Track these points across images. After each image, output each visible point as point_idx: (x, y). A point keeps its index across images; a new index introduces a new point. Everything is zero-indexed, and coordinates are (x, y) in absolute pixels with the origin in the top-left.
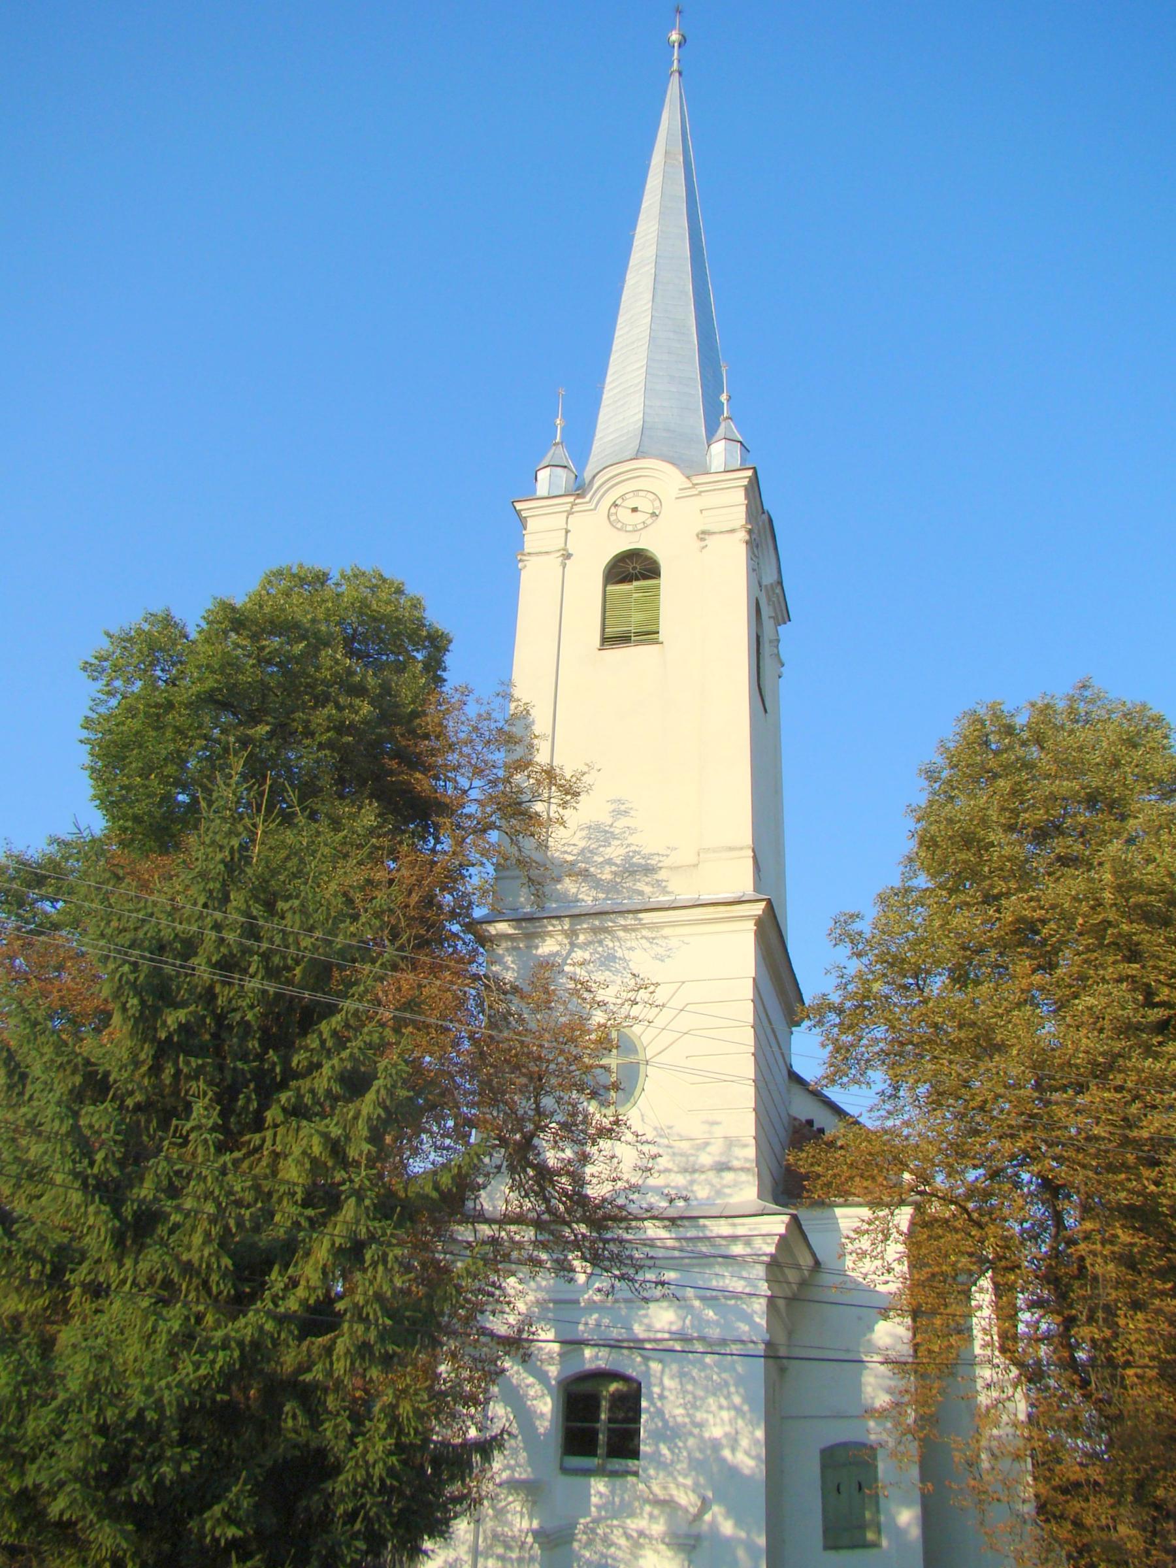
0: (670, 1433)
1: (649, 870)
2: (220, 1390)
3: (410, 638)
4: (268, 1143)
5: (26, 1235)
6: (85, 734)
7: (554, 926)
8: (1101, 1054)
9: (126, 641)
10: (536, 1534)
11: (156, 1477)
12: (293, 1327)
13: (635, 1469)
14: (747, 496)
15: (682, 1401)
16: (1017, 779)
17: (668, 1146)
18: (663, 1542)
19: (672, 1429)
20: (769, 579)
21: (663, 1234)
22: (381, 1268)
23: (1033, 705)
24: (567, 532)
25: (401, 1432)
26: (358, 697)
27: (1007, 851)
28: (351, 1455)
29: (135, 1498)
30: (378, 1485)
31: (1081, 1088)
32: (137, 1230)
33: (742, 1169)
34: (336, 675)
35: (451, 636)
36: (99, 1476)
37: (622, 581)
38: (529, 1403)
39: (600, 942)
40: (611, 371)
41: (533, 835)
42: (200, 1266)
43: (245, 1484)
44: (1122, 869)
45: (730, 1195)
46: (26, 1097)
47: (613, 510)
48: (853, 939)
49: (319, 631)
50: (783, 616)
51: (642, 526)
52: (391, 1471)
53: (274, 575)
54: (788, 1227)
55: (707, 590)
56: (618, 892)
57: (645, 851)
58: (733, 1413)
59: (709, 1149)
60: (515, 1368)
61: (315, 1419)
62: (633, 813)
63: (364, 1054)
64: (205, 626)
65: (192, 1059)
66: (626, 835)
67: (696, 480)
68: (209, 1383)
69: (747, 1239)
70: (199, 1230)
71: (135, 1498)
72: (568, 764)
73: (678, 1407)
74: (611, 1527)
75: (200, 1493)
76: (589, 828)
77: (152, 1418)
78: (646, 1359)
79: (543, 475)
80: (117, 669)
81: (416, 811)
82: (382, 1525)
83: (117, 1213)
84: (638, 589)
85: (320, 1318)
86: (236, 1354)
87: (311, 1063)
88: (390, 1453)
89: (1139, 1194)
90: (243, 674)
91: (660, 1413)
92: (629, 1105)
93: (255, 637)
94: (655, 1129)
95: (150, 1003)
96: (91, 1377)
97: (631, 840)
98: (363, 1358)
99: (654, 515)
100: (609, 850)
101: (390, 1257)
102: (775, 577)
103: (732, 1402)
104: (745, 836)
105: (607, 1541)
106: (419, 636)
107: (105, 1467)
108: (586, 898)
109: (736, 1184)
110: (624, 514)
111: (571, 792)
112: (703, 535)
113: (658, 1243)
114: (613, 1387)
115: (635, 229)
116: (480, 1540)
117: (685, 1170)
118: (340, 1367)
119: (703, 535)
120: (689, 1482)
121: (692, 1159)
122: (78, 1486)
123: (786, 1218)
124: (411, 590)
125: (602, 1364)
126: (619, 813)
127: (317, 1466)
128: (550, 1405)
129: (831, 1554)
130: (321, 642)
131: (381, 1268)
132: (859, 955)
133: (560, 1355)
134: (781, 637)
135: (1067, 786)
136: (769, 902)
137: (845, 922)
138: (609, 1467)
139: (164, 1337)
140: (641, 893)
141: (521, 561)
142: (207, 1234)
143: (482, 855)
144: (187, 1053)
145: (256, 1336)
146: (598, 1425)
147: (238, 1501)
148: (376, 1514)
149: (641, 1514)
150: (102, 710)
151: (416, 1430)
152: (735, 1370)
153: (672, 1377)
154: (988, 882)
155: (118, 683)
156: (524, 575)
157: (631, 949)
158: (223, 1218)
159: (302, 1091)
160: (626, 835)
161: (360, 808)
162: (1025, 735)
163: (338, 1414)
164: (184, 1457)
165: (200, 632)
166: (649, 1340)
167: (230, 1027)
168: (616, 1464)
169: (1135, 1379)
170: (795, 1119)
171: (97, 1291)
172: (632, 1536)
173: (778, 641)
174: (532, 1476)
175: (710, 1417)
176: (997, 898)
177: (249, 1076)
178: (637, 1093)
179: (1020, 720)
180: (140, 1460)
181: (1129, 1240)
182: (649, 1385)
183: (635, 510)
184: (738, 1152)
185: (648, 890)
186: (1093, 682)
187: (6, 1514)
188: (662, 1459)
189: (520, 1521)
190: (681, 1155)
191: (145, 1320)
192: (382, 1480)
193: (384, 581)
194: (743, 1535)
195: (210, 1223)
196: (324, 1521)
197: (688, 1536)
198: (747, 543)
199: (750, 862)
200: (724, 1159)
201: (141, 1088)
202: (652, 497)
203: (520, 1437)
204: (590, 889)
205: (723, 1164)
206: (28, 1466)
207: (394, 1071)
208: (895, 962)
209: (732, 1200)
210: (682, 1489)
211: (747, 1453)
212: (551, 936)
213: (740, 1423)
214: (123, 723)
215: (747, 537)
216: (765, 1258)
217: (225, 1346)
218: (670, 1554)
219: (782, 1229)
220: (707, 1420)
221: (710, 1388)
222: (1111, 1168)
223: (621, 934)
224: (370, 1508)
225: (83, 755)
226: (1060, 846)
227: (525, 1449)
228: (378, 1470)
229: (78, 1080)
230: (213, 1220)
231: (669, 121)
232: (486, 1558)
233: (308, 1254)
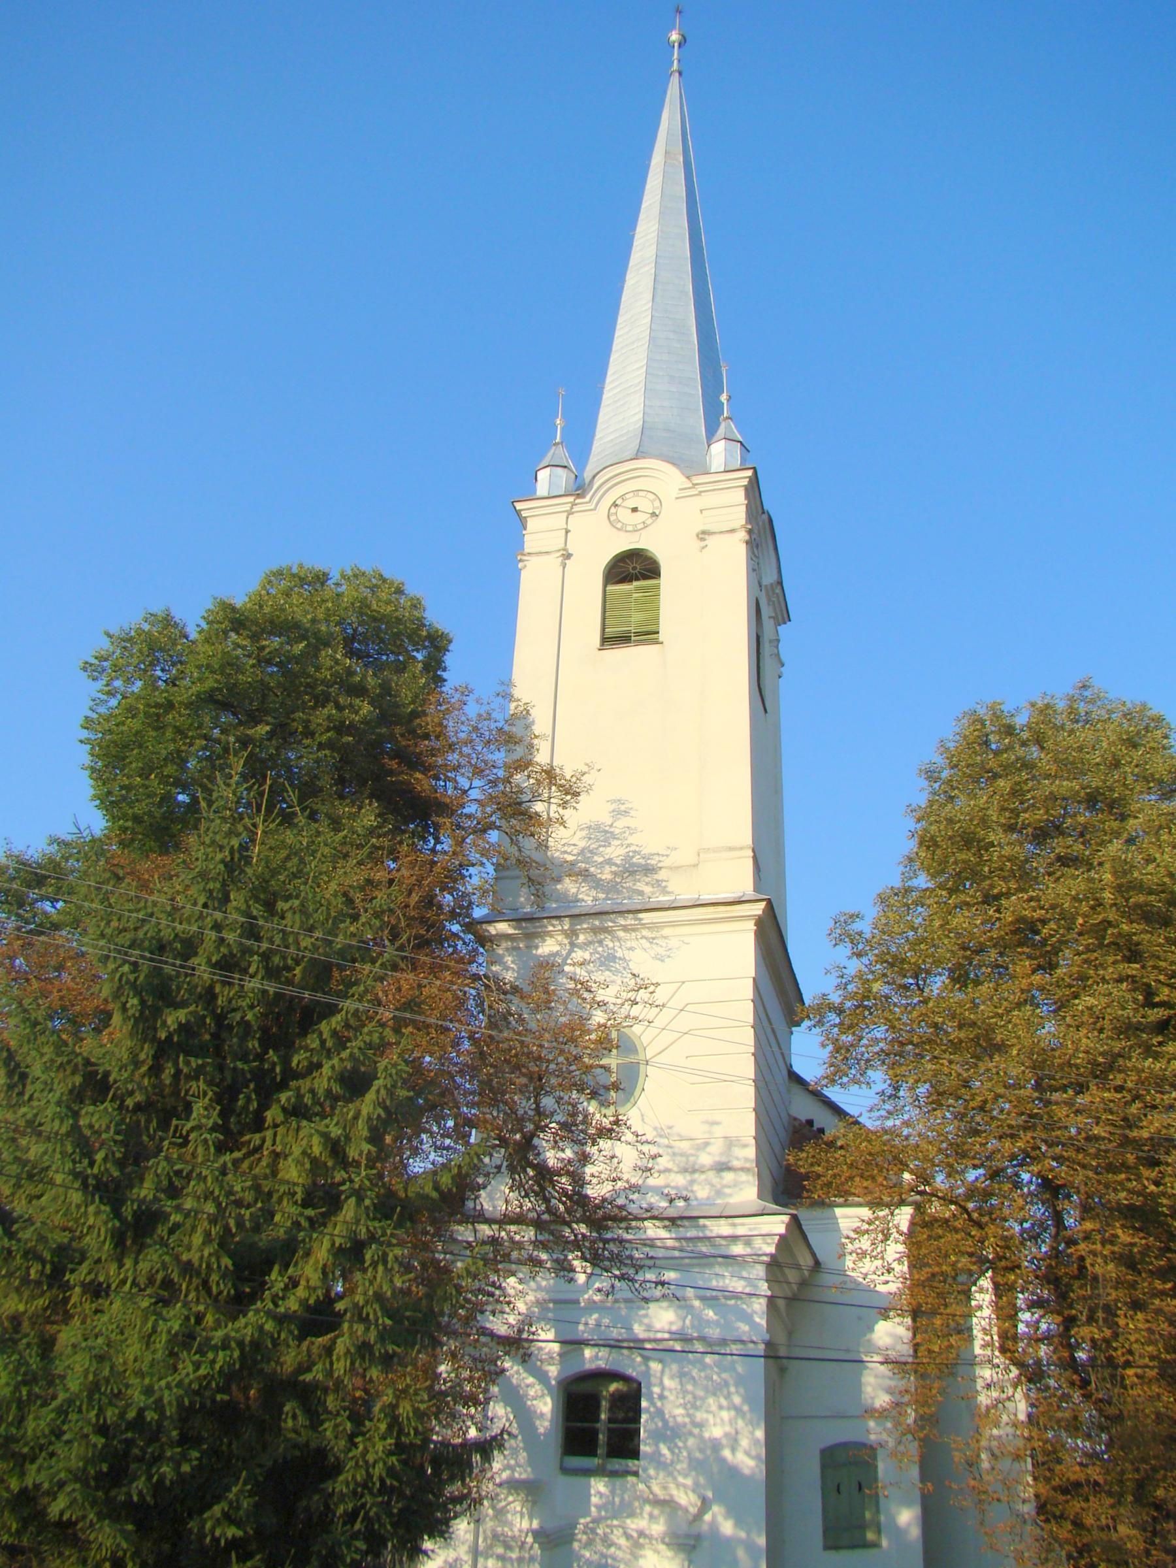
0: (670, 1433)
1: (649, 870)
4: (268, 1143)
5: (26, 1235)
6: (85, 734)
7: (554, 926)
8: (1101, 1054)
9: (126, 641)
10: (536, 1534)
11: (156, 1477)
12: (293, 1327)
13: (635, 1469)
14: (747, 496)
15: (682, 1401)
16: (1017, 779)
17: (668, 1146)
18: (663, 1542)
19: (672, 1429)
20: (769, 578)
21: (663, 1233)
22: (381, 1268)
23: (1033, 705)
24: (567, 532)
25: (401, 1431)
26: (358, 697)
27: (1007, 851)
28: (350, 1455)
29: (135, 1498)
30: (378, 1485)
31: (1081, 1088)
32: (137, 1230)
33: (742, 1169)
34: (336, 675)
35: (451, 636)
36: (99, 1476)
38: (529, 1403)
39: (600, 942)
40: (610, 372)
41: (533, 835)
42: (200, 1266)
43: (245, 1484)
44: (1122, 869)
45: (730, 1195)
46: (26, 1097)
47: (613, 510)
48: (853, 939)
49: (319, 631)
50: (783, 616)
51: (642, 526)
52: (391, 1471)
53: (274, 574)
54: (788, 1226)
55: (707, 591)
56: (619, 892)
58: (733, 1413)
59: (709, 1149)
60: (515, 1368)
61: (315, 1419)
62: (632, 813)
63: (364, 1054)
64: (205, 626)
65: (192, 1059)
67: (696, 480)
68: (209, 1383)
69: (747, 1240)
70: (199, 1230)
71: (135, 1498)
72: (568, 764)
73: (678, 1407)
74: (611, 1527)
75: (201, 1492)
76: (589, 828)
78: (646, 1359)
79: (543, 475)
80: (116, 668)
81: (416, 811)
82: (382, 1525)
83: (117, 1213)
84: (638, 589)
85: (320, 1318)
86: (236, 1354)
87: (311, 1063)
88: (390, 1453)
90: (243, 673)
91: (660, 1413)
92: (629, 1105)
93: (255, 637)
94: (655, 1129)
95: (150, 1003)
96: (91, 1377)
97: (630, 840)
98: (363, 1358)
99: (654, 515)
100: (609, 850)
101: (390, 1257)
104: (745, 836)
105: (607, 1541)
106: (419, 636)
108: (586, 898)
110: (624, 514)
111: (571, 792)
112: (703, 535)
113: (658, 1243)
114: (613, 1387)
116: (480, 1540)
117: (685, 1170)
118: (340, 1367)
119: (703, 535)
120: (689, 1482)
122: (78, 1486)
123: (786, 1218)
124: (411, 590)
125: (602, 1364)
126: (619, 813)
127: (318, 1466)
128: (550, 1405)
129: (832, 1554)
131: (381, 1268)
132: (859, 955)
133: (560, 1355)
134: (781, 637)
135: (1066, 786)
136: (769, 903)
138: (609, 1467)
139: (164, 1337)
140: (641, 893)
141: (521, 561)
142: (207, 1234)
143: (482, 855)
144: (187, 1053)
146: (598, 1425)
147: (238, 1501)
148: (376, 1514)
149: (641, 1514)
150: (102, 710)
151: (416, 1429)
152: (735, 1369)
153: (672, 1377)
154: (988, 882)
155: (118, 683)
157: (631, 949)
159: (302, 1091)
161: (360, 808)
162: (1025, 735)
163: (338, 1414)
164: (185, 1457)
165: (200, 632)
166: (649, 1340)
167: (230, 1028)
168: (616, 1464)
169: (1135, 1379)
170: (795, 1119)
171: (97, 1291)
172: (632, 1536)
173: (778, 641)
174: (532, 1476)
175: (710, 1417)
176: (997, 898)
177: (249, 1076)
178: (637, 1093)
179: (1021, 720)
181: (1129, 1240)
182: (649, 1385)
183: (635, 510)
184: (738, 1152)
185: (648, 890)
186: (1094, 682)
188: (662, 1459)
189: (520, 1521)
190: (681, 1155)
191: (145, 1320)
192: (382, 1480)
193: (384, 581)
194: (743, 1535)
195: (210, 1222)
196: (324, 1521)
197: (688, 1536)
198: (747, 543)
199: (750, 862)
200: (724, 1159)
201: (141, 1088)
202: (652, 497)
203: (520, 1437)
205: (723, 1164)
206: (28, 1466)
207: (394, 1071)
208: (895, 962)
209: (732, 1200)
211: (747, 1453)
212: (552, 936)
213: (740, 1423)
214: (123, 723)
215: (747, 537)
216: (765, 1258)
217: (225, 1346)
218: (670, 1554)
219: (782, 1229)
220: (707, 1420)
221: (710, 1388)
222: (1111, 1168)
223: (621, 934)
224: (370, 1508)
225: (83, 755)
226: (1060, 846)
227: (525, 1449)
228: (378, 1470)
229: (78, 1080)
230: (213, 1220)
231: (669, 121)
232: (486, 1558)
233: (308, 1254)
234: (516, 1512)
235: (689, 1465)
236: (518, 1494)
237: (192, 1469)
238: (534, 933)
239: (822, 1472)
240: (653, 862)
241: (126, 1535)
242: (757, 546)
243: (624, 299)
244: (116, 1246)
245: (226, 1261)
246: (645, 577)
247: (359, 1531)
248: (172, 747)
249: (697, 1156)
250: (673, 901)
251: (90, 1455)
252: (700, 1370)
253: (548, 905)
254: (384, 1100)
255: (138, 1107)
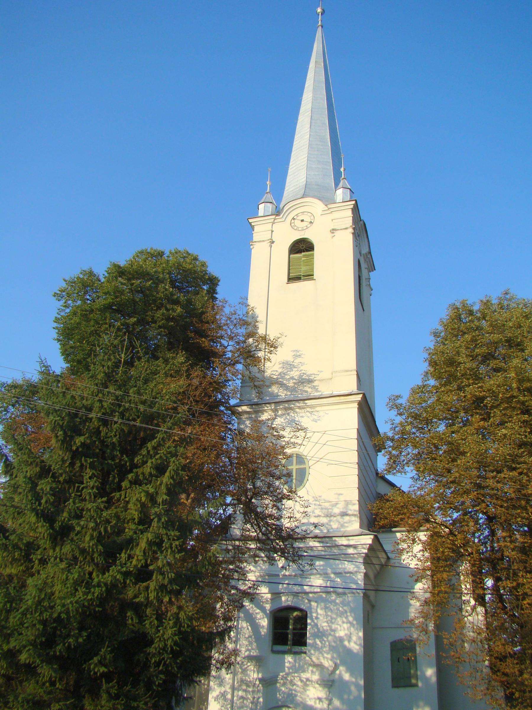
0: (320, 634)
1: (310, 381)
2: (98, 606)
3: (201, 279)
4: (123, 497)
5: (12, 537)
6: (55, 325)
7: (267, 407)
8: (508, 454)
9: (72, 283)
10: (260, 680)
11: (67, 644)
12: (132, 578)
13: (305, 651)
14: (353, 213)
15: (326, 620)
16: (474, 334)
17: (319, 505)
18: (318, 683)
19: (321, 632)
20: (365, 251)
21: (317, 544)
22: (169, 551)
23: (481, 301)
24: (272, 231)
25: (181, 626)
26: (175, 305)
27: (468, 365)
28: (157, 635)
29: (58, 654)
30: (170, 649)
31: (499, 472)
32: (60, 535)
33: (353, 515)
34: (166, 295)
35: (219, 278)
36: (41, 643)
37: (297, 253)
38: (257, 621)
39: (288, 414)
40: (292, 160)
41: (256, 366)
42: (89, 550)
43: (108, 647)
44: (519, 372)
45: (347, 527)
46: (14, 476)
47: (293, 221)
48: (397, 407)
49: (159, 277)
50: (372, 268)
52: (176, 643)
53: (140, 253)
54: (373, 540)
55: (336, 257)
56: (296, 392)
57: (308, 373)
58: (349, 625)
59: (338, 506)
60: (251, 605)
61: (141, 618)
62: (302, 356)
63: (166, 457)
64: (107, 275)
65: (88, 459)
67: (330, 206)
68: (93, 603)
69: (355, 547)
70: (88, 534)
71: (58, 654)
72: (272, 336)
73: (324, 622)
74: (294, 677)
75: (88, 651)
76: (283, 363)
77: (64, 617)
78: (310, 601)
79: (261, 207)
80: (69, 295)
81: (203, 356)
82: (173, 668)
83: (52, 527)
84: (304, 256)
85: (143, 574)
86: (104, 589)
87: (143, 461)
88: (175, 634)
89: (527, 519)
90: (124, 295)
91: (316, 625)
92: (301, 487)
93: (129, 279)
94: (313, 497)
95: (69, 434)
96: (37, 598)
97: (302, 368)
98: (162, 592)
99: (311, 222)
100: (292, 373)
101: (174, 545)
102: (368, 250)
103: (348, 620)
104: (352, 364)
105: (292, 683)
106: (205, 278)
107: (44, 639)
108: (282, 394)
109: (350, 522)
110: (297, 223)
111: (273, 346)
112: (333, 231)
113: (315, 549)
114: (295, 614)
116: (236, 683)
117: (327, 516)
118: (152, 596)
119: (333, 231)
120: (329, 656)
121: (330, 510)
122: (31, 647)
123: (372, 537)
124: (201, 258)
125: (290, 603)
126: (297, 356)
127: (143, 640)
128: (266, 622)
129: (396, 690)
130: (158, 281)
131: (169, 551)
132: (401, 414)
133: (271, 599)
134: (371, 277)
135: (496, 337)
136: (364, 397)
137: (394, 399)
138: (293, 650)
139: (71, 581)
140: (307, 392)
141: (251, 245)
142: (92, 536)
143: (233, 375)
144: (86, 457)
145: (113, 581)
146: (289, 631)
147: (105, 655)
148: (170, 662)
149: (308, 671)
150: (63, 314)
151: (188, 625)
152: (350, 606)
153: (321, 609)
154: (460, 380)
155: (70, 302)
156: (253, 251)
157: (302, 417)
158: (98, 528)
159: (139, 474)
161: (177, 354)
162: (479, 315)
163: (151, 617)
164: (80, 635)
165: (105, 278)
166: (311, 593)
167: (107, 446)
168: (297, 649)
169: (527, 606)
170: (379, 494)
171: (43, 562)
172: (303, 681)
173: (370, 279)
174: (258, 654)
175: (339, 627)
176: (463, 387)
177: (114, 467)
178: (305, 482)
179: (476, 308)
180: (60, 636)
181: (522, 540)
182: (311, 612)
183: (302, 221)
184: (350, 507)
185: (309, 390)
186: (510, 291)
187: (2, 661)
188: (317, 646)
189: (254, 674)
190: (325, 509)
191: (63, 573)
192: (172, 648)
193: (189, 254)
194: (354, 680)
195: (93, 530)
196: (146, 665)
197: (328, 681)
198: (353, 234)
199: (355, 376)
200: (344, 510)
201: (65, 472)
203: (253, 637)
205: (344, 512)
206: (11, 639)
207: (177, 463)
208: (416, 417)
209: (348, 529)
210: (326, 659)
211: (355, 643)
212: (266, 412)
213: (352, 629)
214: (72, 319)
215: (353, 231)
216: (363, 555)
217: (99, 585)
218: (320, 689)
219: (370, 542)
220: (337, 628)
221: (339, 613)
222: (514, 507)
223: (298, 410)
224: (167, 661)
225: (54, 334)
226: (493, 363)
227: (255, 642)
228: (169, 642)
229: (38, 469)
230: (94, 529)
231: (317, 47)
232: (238, 691)
233: (137, 545)
234: (251, 670)
235: (329, 648)
236: (252, 662)
237: (83, 640)
239: (391, 653)
241: (55, 671)
242: (359, 236)
244: (52, 543)
245: (100, 547)
246: (308, 251)
247: (162, 670)
248: (93, 328)
249: (332, 509)
250: (321, 395)
251: (37, 633)
252: (334, 606)
253: (265, 398)
254: (173, 476)
255: (65, 481)
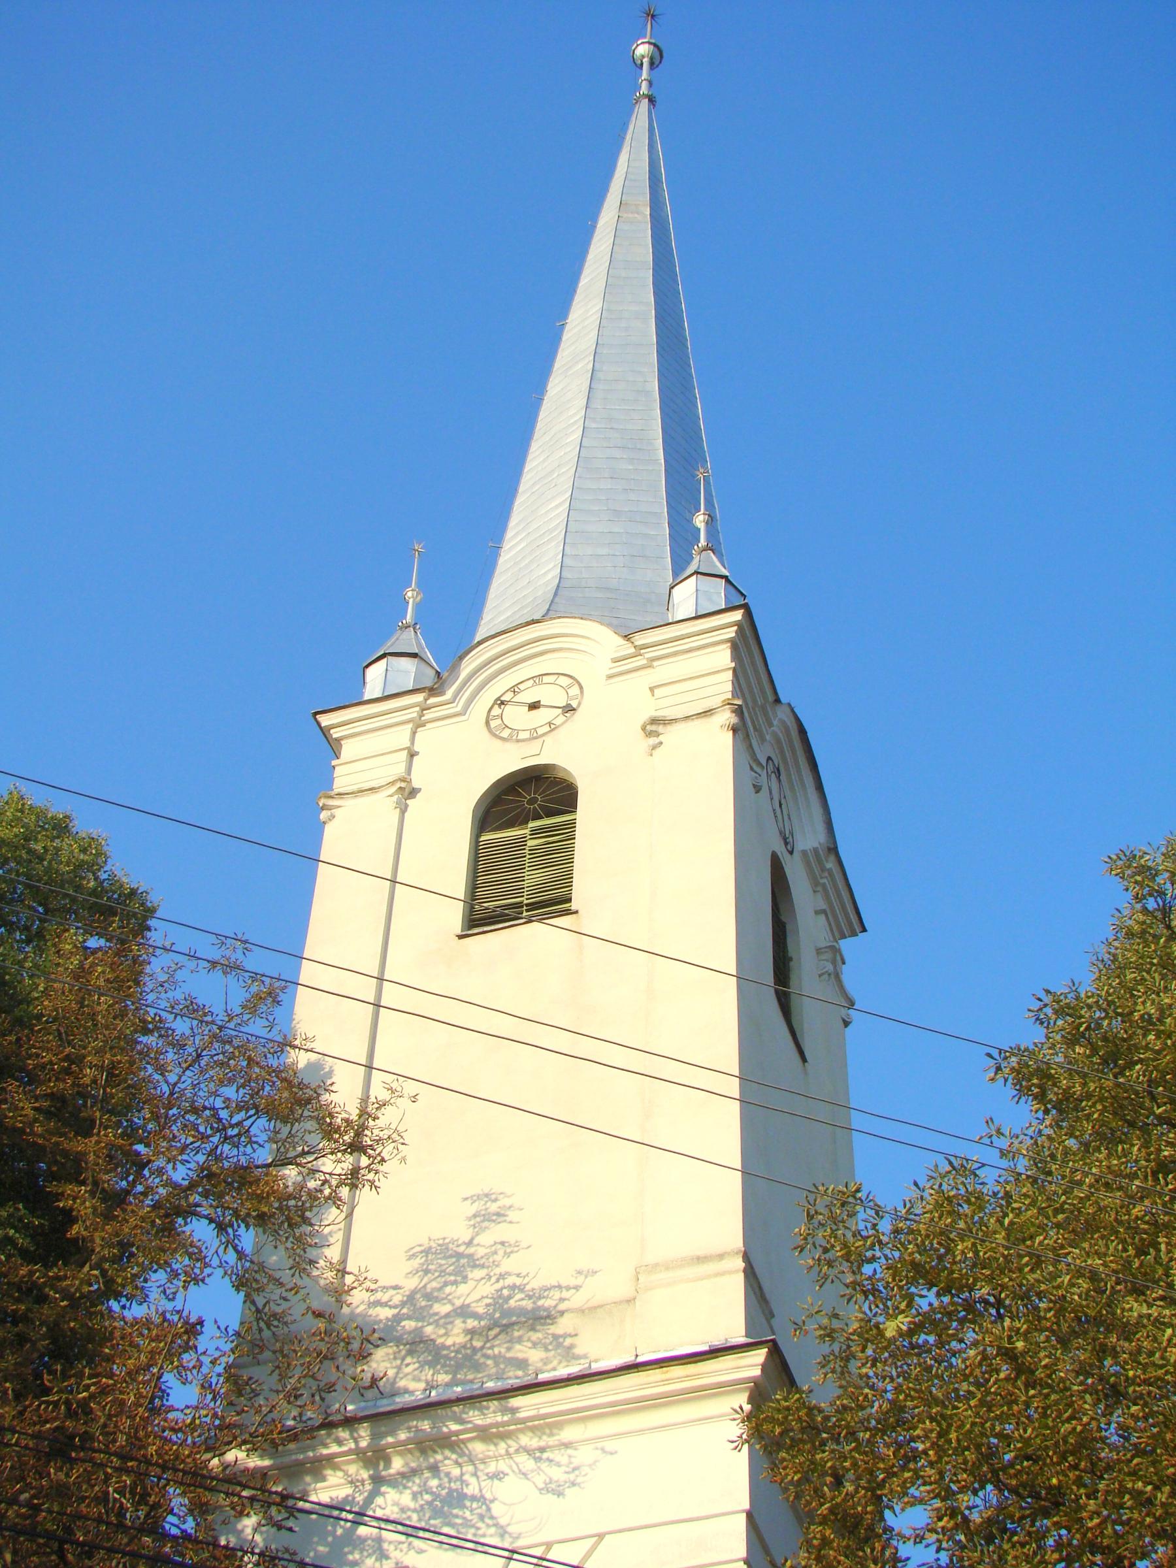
1: (539, 1318)
7: (340, 1442)
20: (810, 838)
39: (435, 1469)
47: (496, 711)
51: (547, 728)
56: (477, 1367)
57: (534, 1284)
62: (512, 1215)
66: (497, 1258)
67: (640, 639)
76: (427, 1252)
84: (535, 832)
97: (507, 1265)
100: (463, 1289)
108: (412, 1385)
110: (517, 716)
112: (654, 726)
115: (566, 317)
119: (654, 726)
140: (522, 1364)
157: (498, 1476)
160: (497, 1258)
183: (534, 706)
185: (535, 1356)
198: (735, 730)
202: (564, 681)
204: (422, 1367)
212: (336, 1467)
215: (733, 719)
223: (478, 1447)
231: (631, 162)
238: (301, 1464)
240: (548, 1303)
243: (543, 414)
246: (551, 813)
